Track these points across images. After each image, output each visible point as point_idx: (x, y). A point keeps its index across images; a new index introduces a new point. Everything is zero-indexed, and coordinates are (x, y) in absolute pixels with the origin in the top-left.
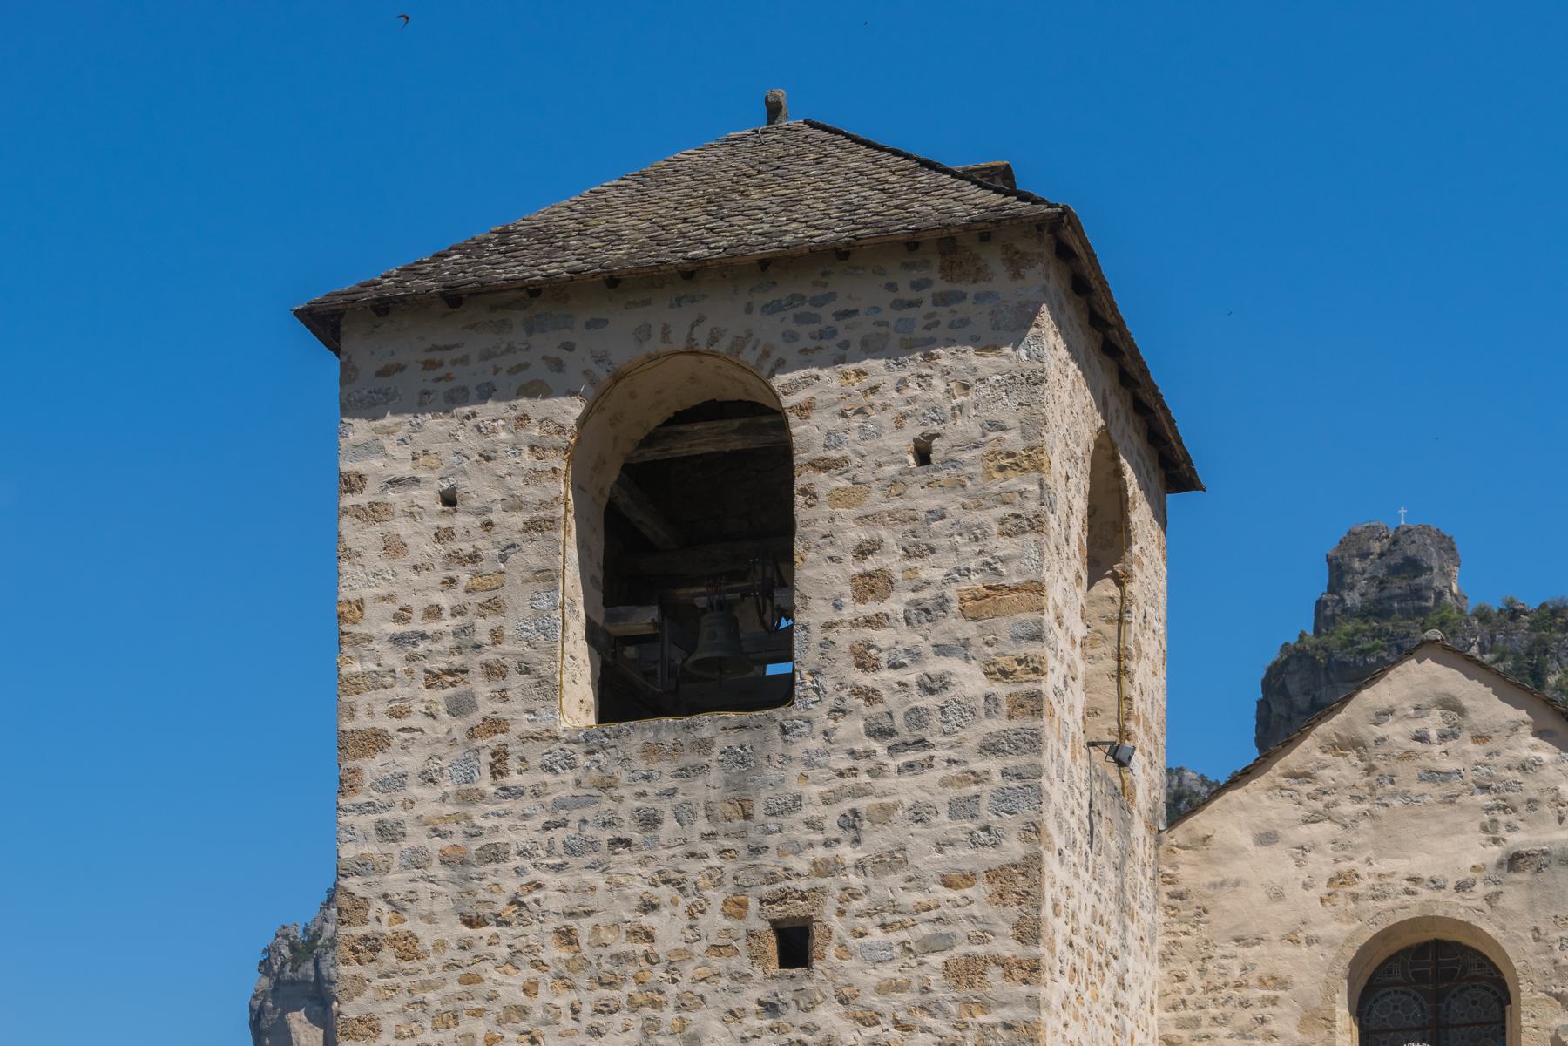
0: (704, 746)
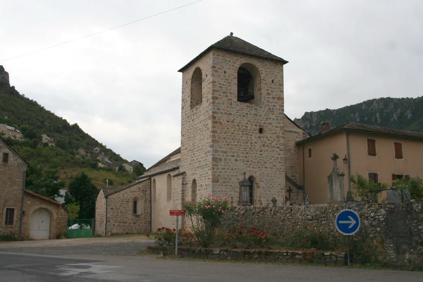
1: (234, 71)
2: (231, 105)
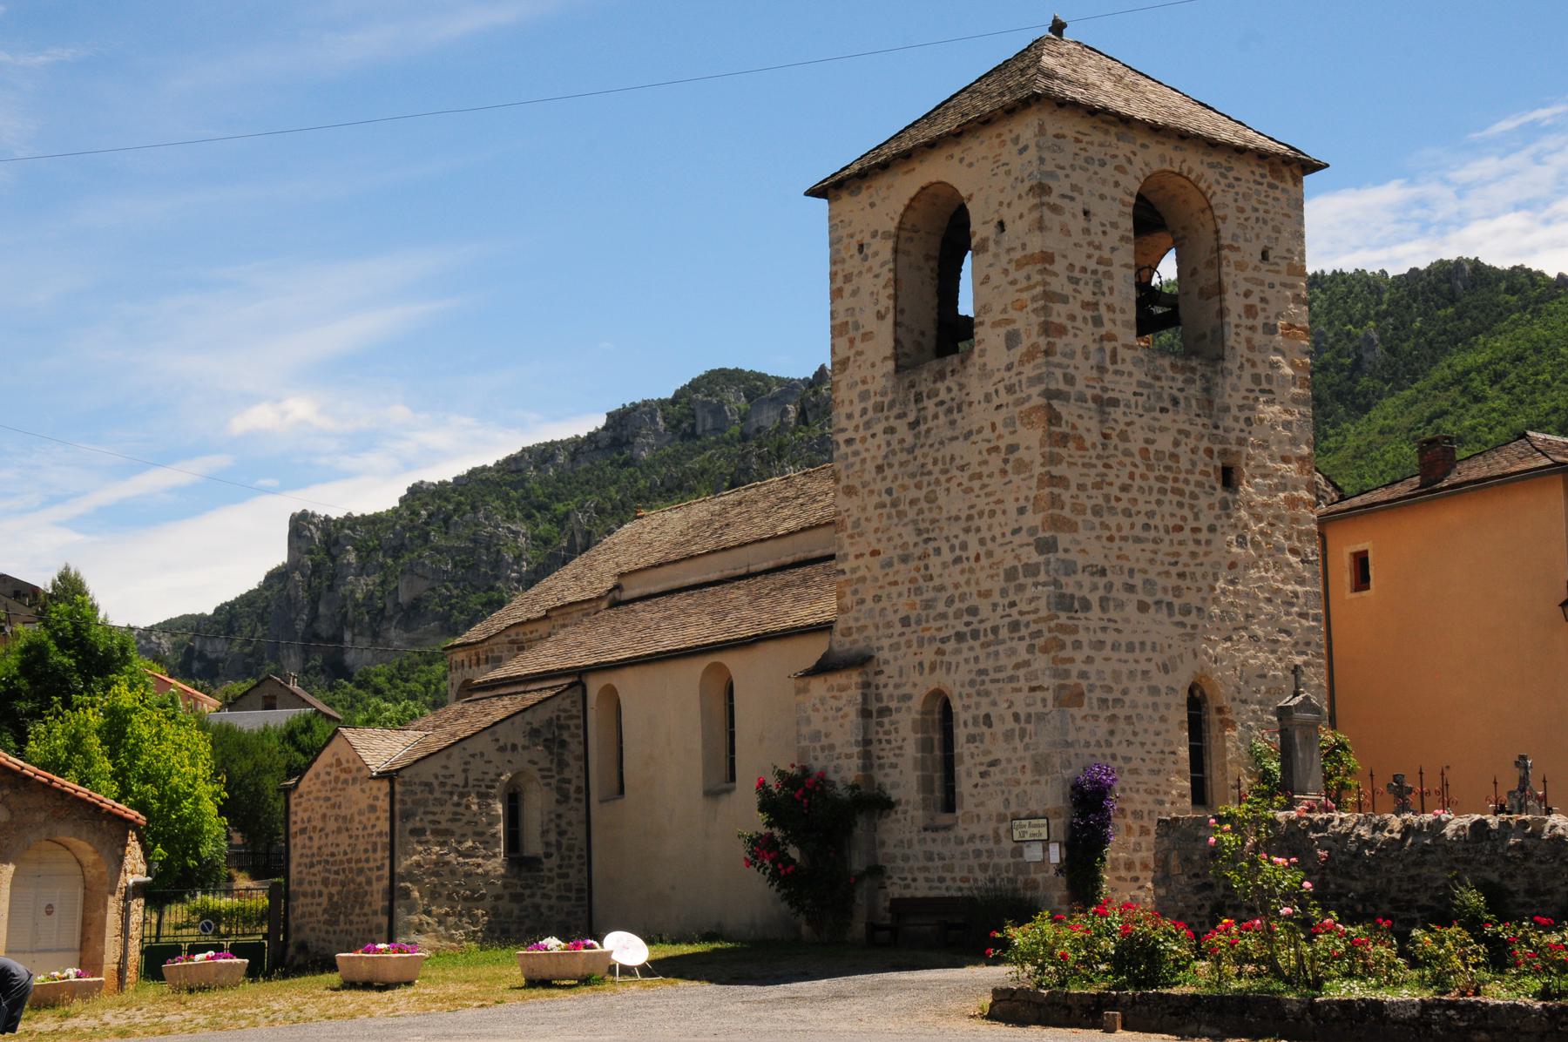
0: (1193, 370)
1: (1117, 206)
2: (1114, 362)
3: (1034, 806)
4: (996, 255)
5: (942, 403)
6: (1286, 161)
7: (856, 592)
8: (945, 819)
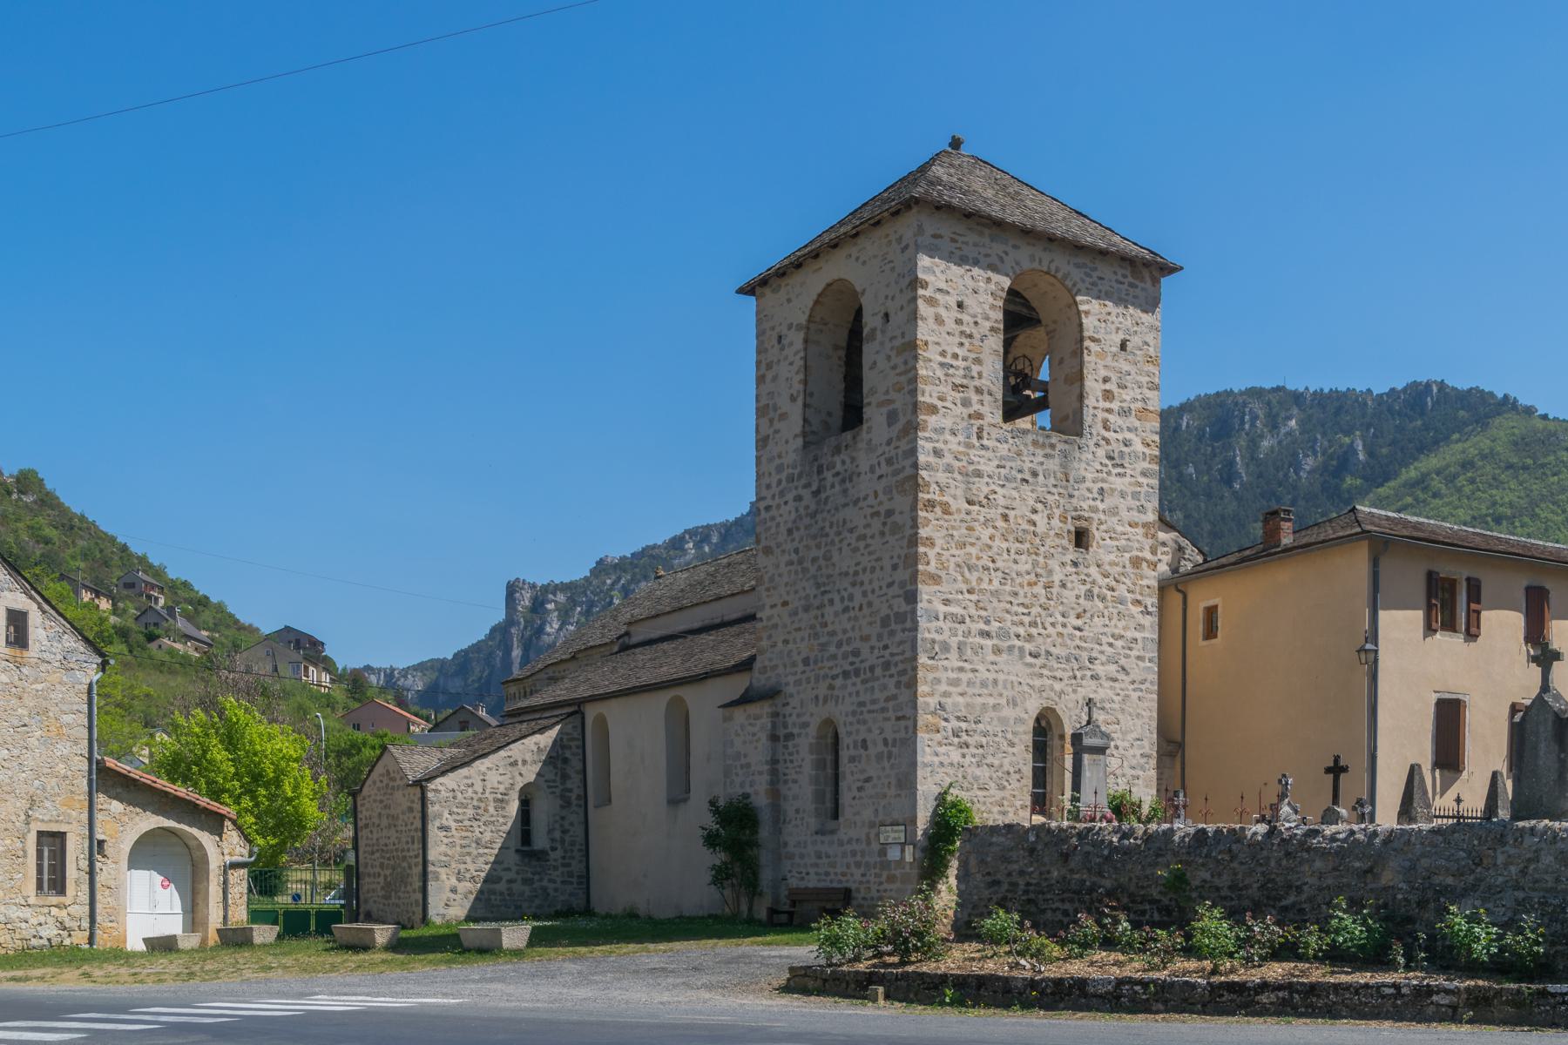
0: (1053, 446)
2: (979, 437)
3: (896, 816)
4: (882, 343)
5: (838, 474)
6: (1147, 264)
7: (770, 637)
8: (831, 824)
